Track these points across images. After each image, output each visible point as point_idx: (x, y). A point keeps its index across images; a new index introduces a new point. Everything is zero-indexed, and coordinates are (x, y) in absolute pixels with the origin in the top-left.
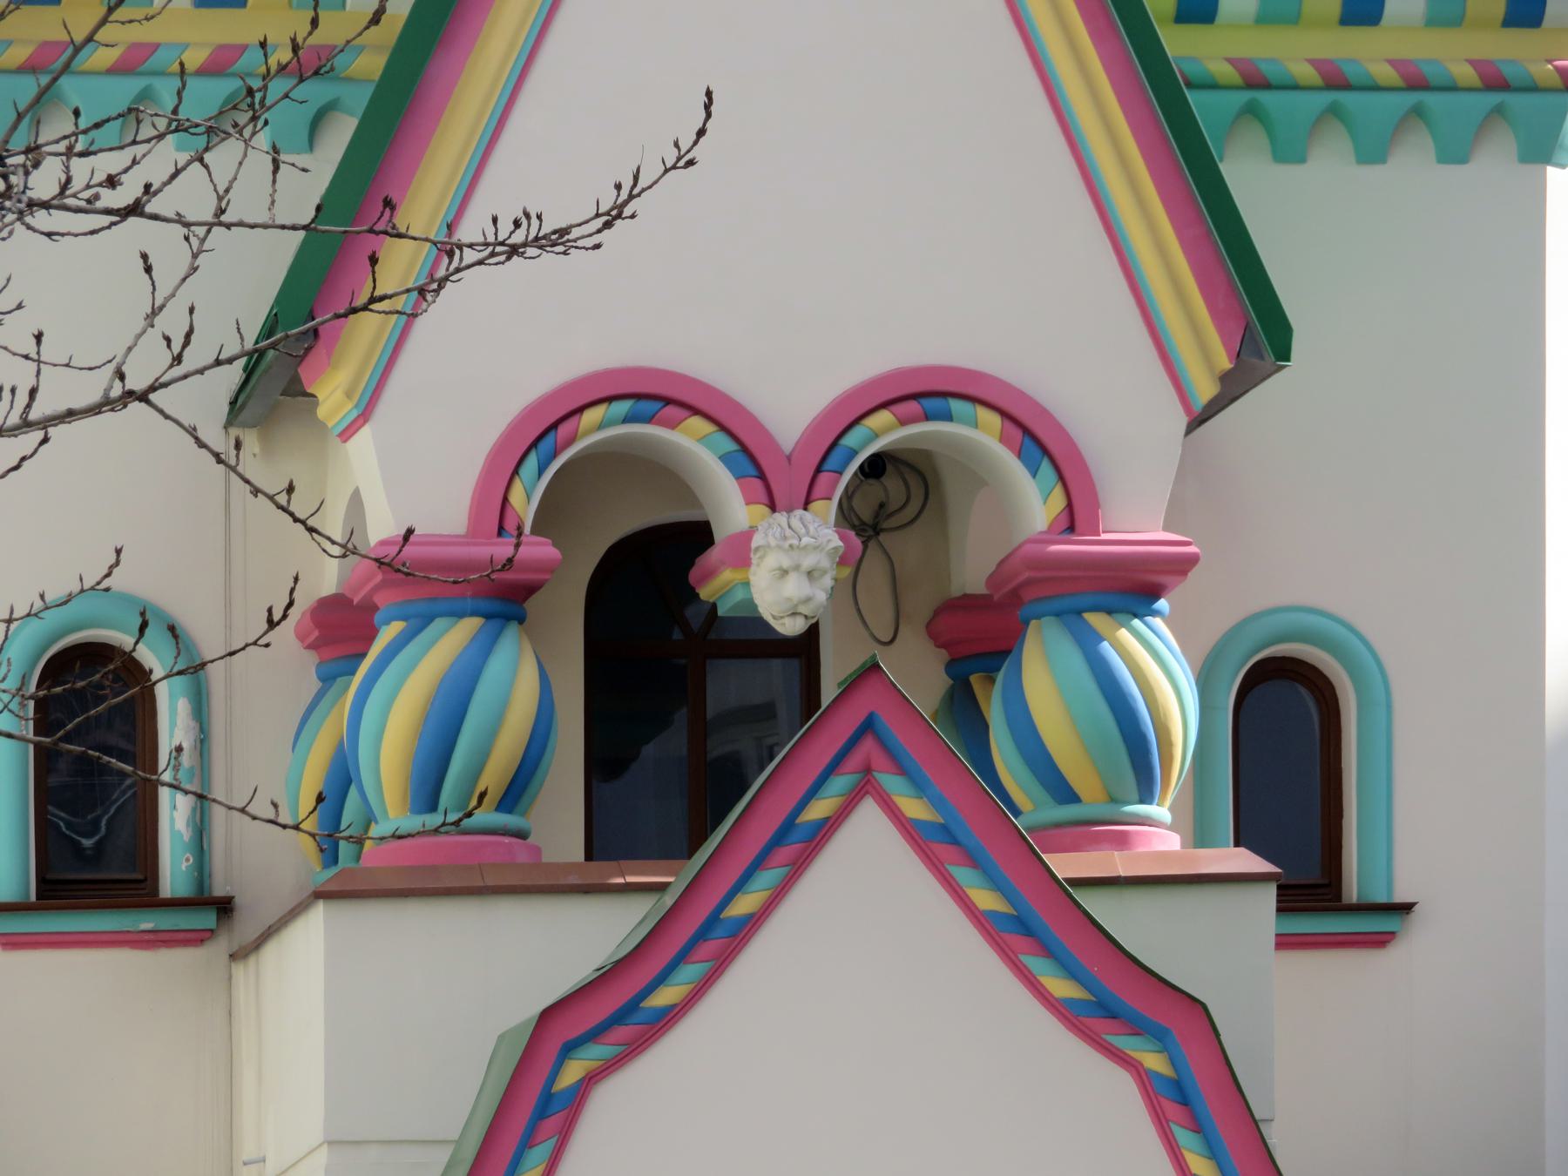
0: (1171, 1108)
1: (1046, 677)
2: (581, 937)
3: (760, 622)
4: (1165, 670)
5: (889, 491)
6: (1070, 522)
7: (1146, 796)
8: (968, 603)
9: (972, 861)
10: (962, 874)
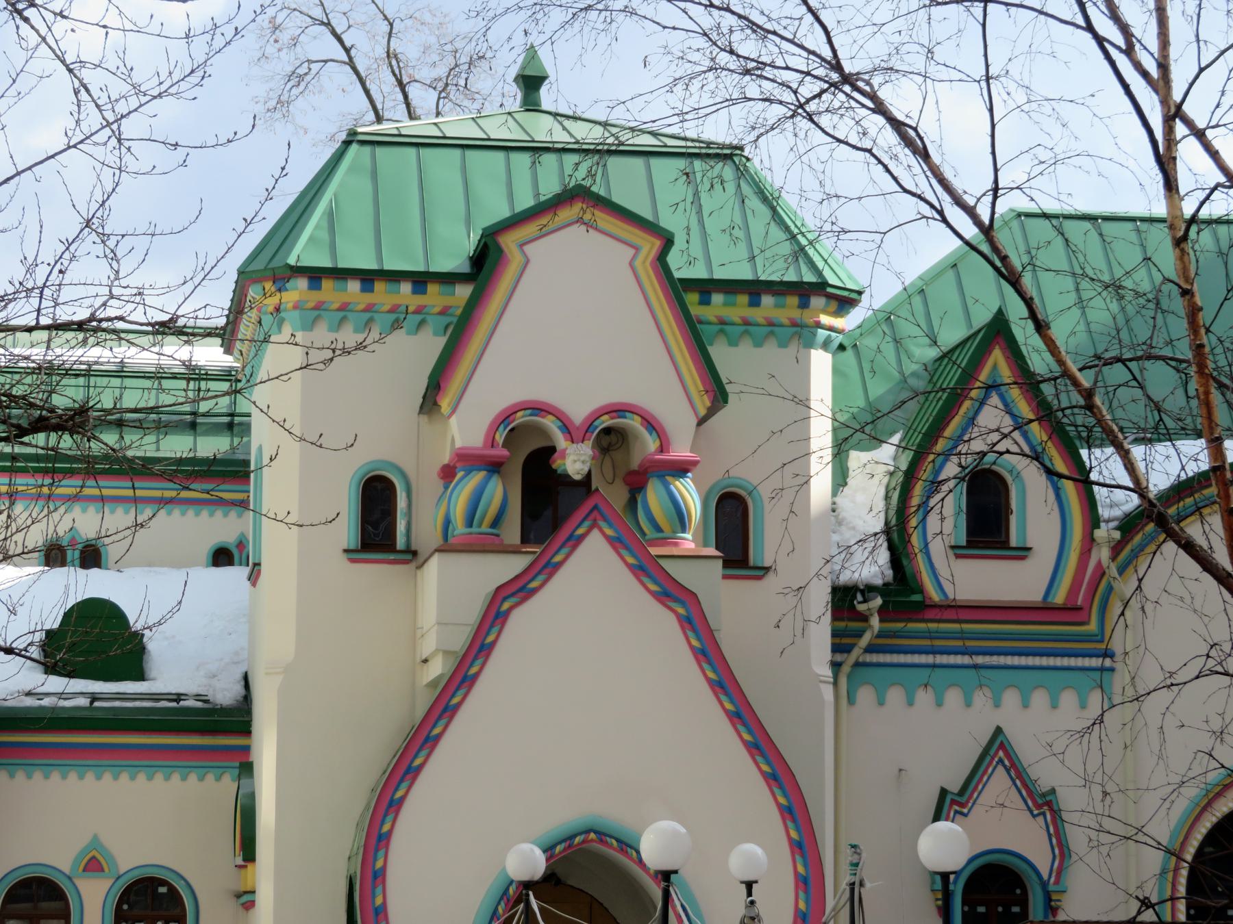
0: (686, 625)
1: (654, 495)
2: (509, 567)
3: (568, 476)
4: (690, 494)
5: (610, 438)
6: (662, 449)
7: (684, 531)
8: (632, 473)
9: (627, 548)
10: (623, 552)
